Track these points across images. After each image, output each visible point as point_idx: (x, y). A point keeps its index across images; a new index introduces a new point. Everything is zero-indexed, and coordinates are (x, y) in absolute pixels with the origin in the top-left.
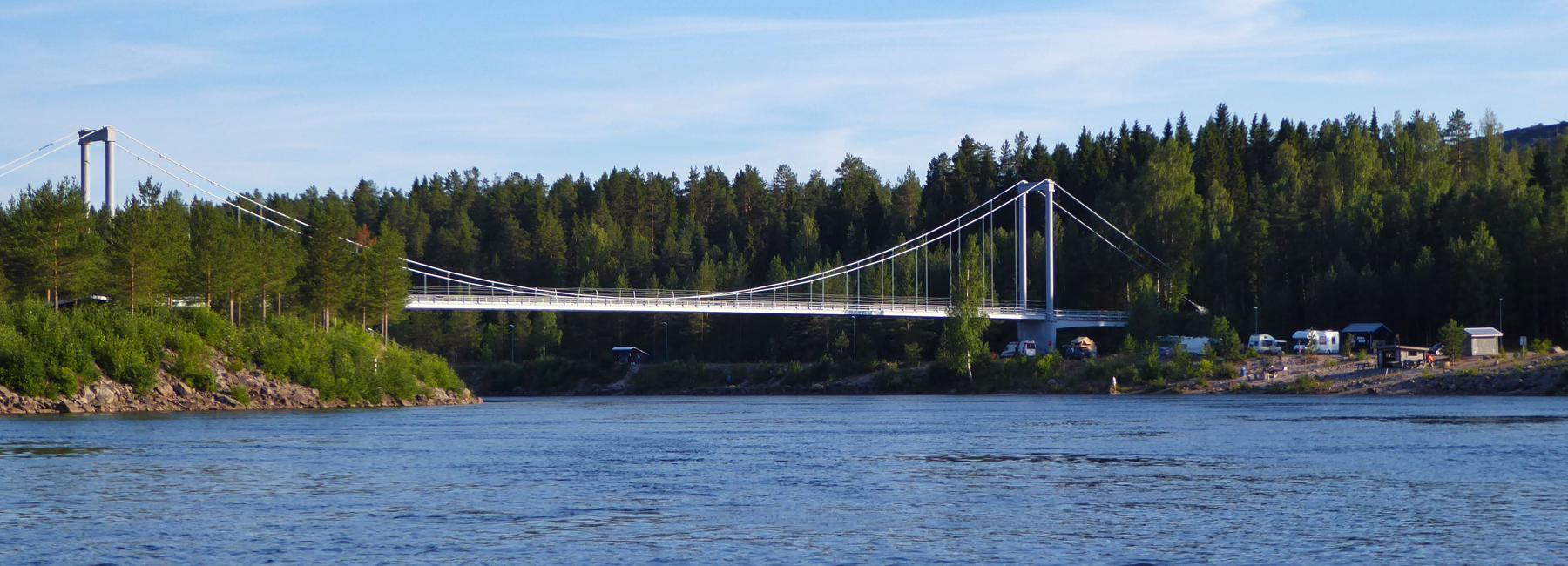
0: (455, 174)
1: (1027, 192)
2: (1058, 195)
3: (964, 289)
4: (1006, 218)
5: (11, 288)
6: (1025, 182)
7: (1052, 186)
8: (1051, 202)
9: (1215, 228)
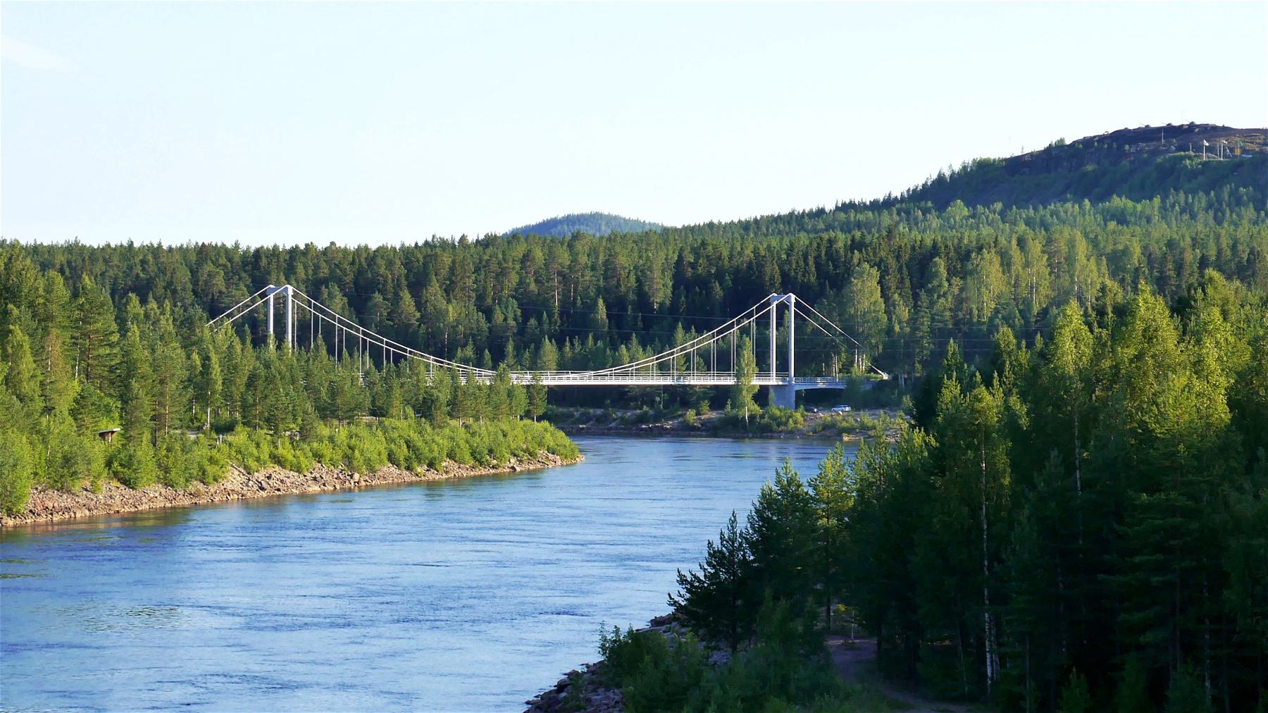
0: (182, 245)
1: (274, 294)
2: (797, 304)
3: (743, 369)
4: (763, 322)
5: (120, 441)
6: (775, 295)
7: (290, 289)
8: (793, 308)
9: (896, 324)
